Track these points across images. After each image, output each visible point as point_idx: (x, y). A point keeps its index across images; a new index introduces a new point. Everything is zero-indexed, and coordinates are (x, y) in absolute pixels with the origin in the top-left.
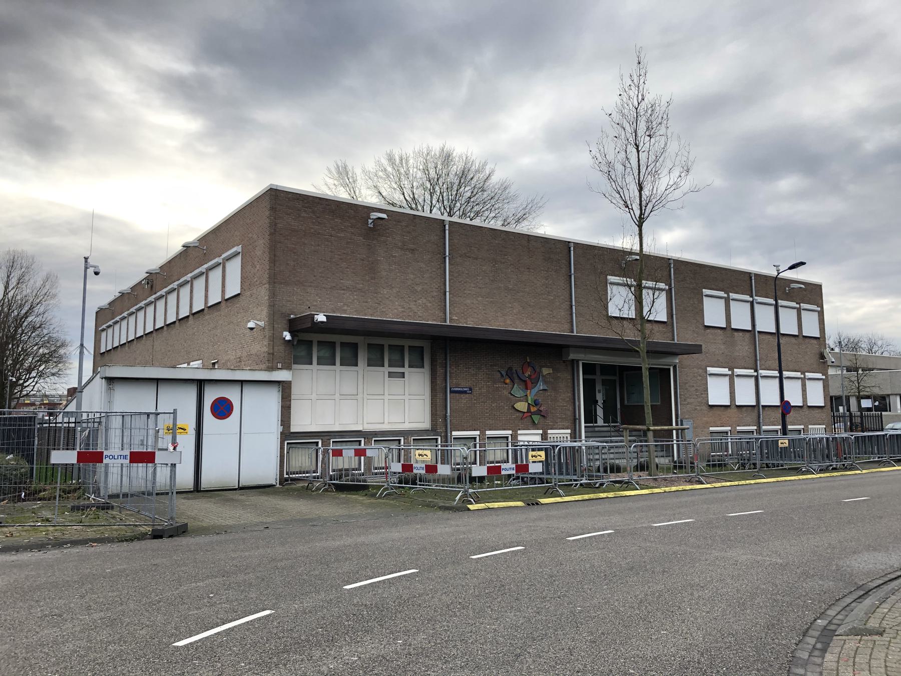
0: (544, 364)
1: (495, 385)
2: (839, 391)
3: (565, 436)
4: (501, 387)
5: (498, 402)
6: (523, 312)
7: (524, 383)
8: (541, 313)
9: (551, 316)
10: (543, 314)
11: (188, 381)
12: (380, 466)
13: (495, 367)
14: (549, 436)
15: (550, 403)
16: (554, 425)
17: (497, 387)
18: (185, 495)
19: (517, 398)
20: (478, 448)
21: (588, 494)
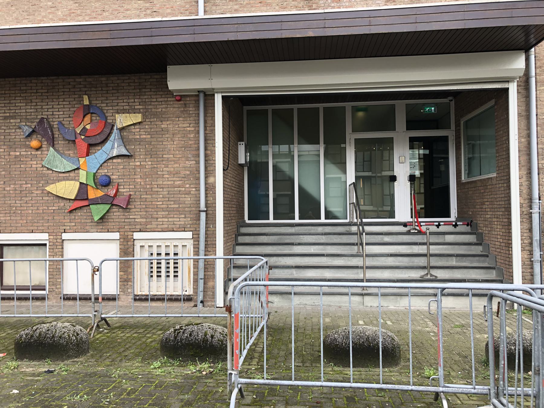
0: (127, 107)
1: (12, 153)
2: (541, 109)
3: (180, 244)
4: (26, 156)
5: (20, 182)
6: (79, 12)
7: (37, 147)
8: (122, 9)
9: (149, 12)
10: (127, 10)
11: (525, 158)
12: (97, 292)
13: (11, 121)
14: (138, 245)
15: (139, 180)
16: (146, 224)
17: (16, 157)
18: (477, 258)
19: (61, 175)
20: (202, 256)
21: (406, 313)
